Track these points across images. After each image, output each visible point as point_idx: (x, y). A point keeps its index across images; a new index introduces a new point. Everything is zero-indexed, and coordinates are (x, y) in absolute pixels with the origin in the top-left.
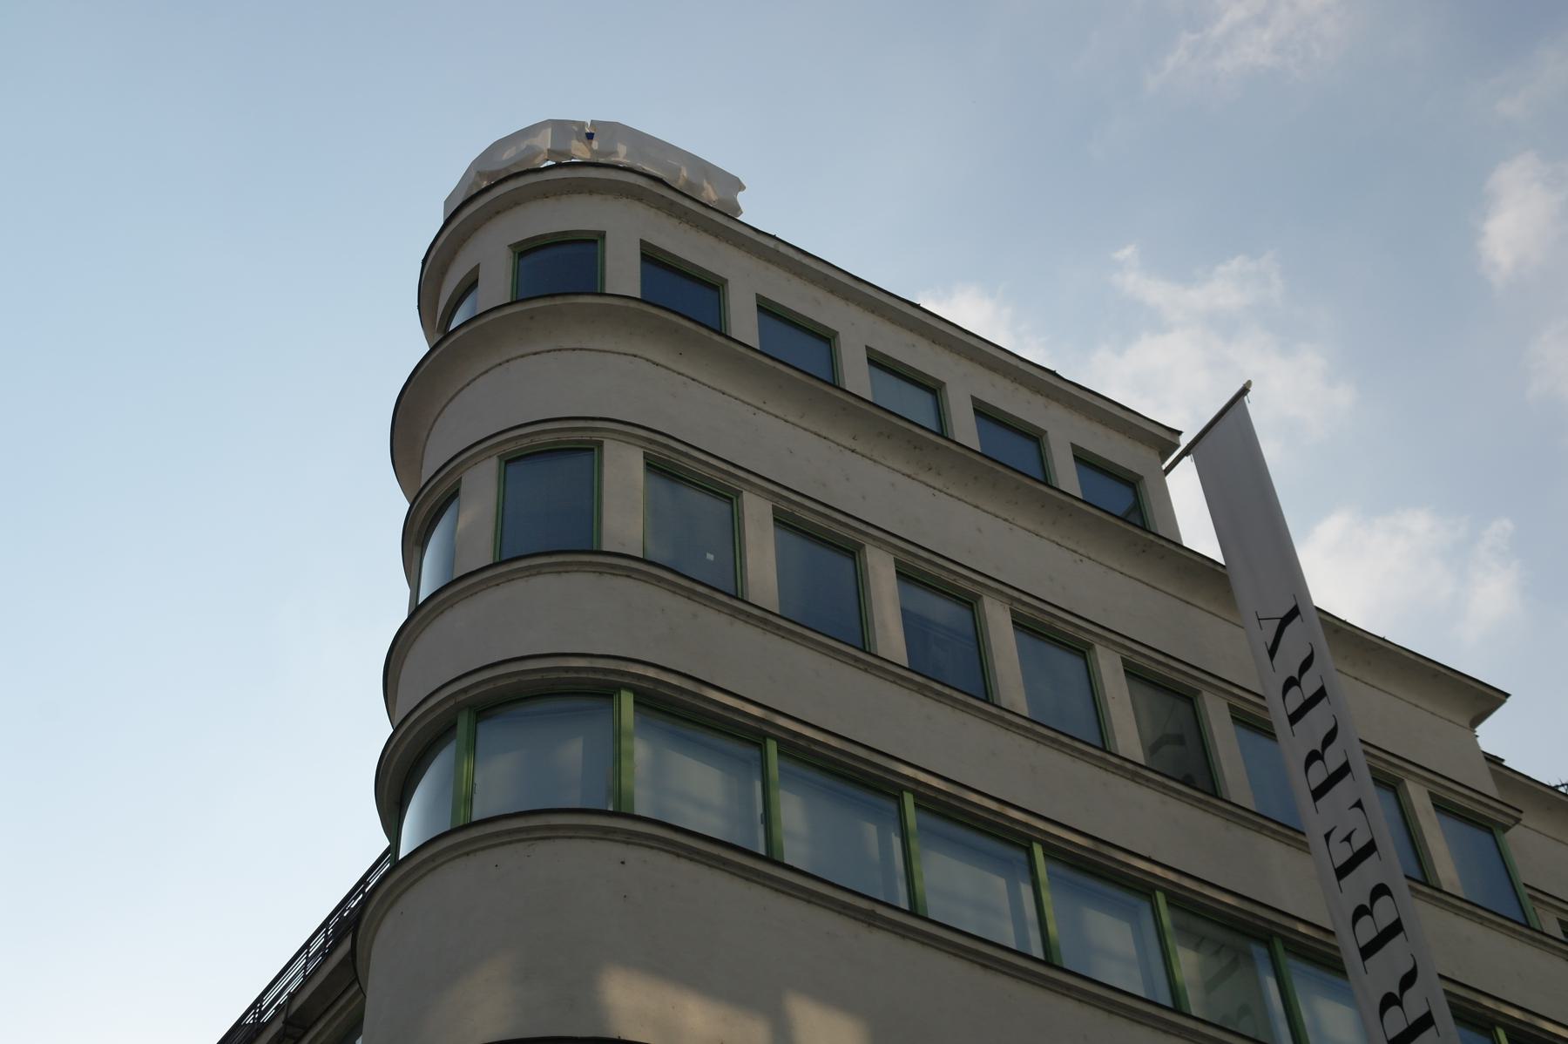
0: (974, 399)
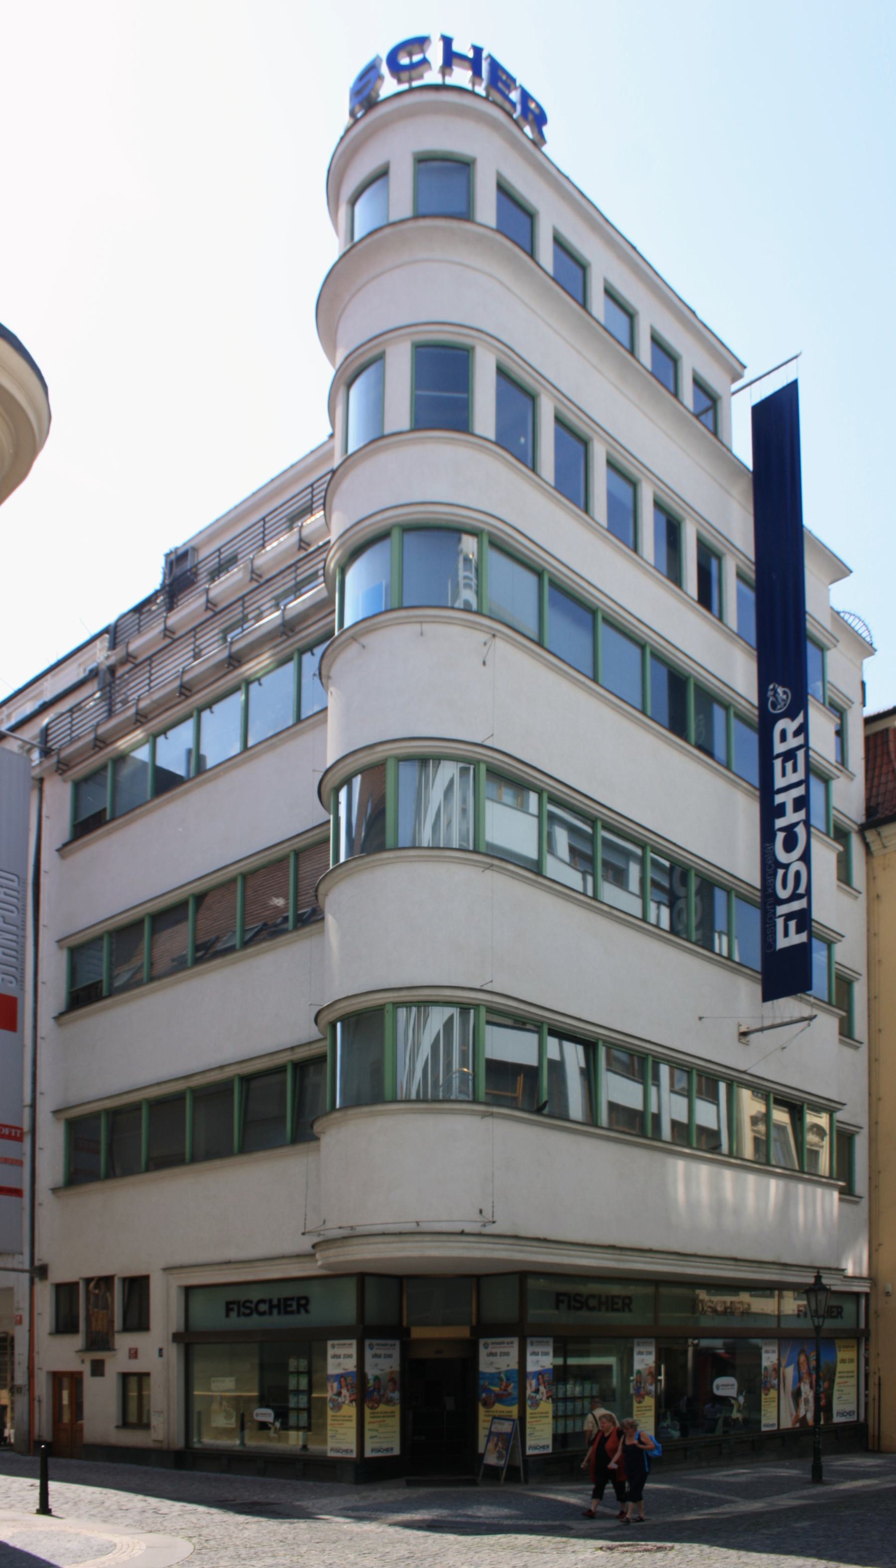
0: (606, 281)
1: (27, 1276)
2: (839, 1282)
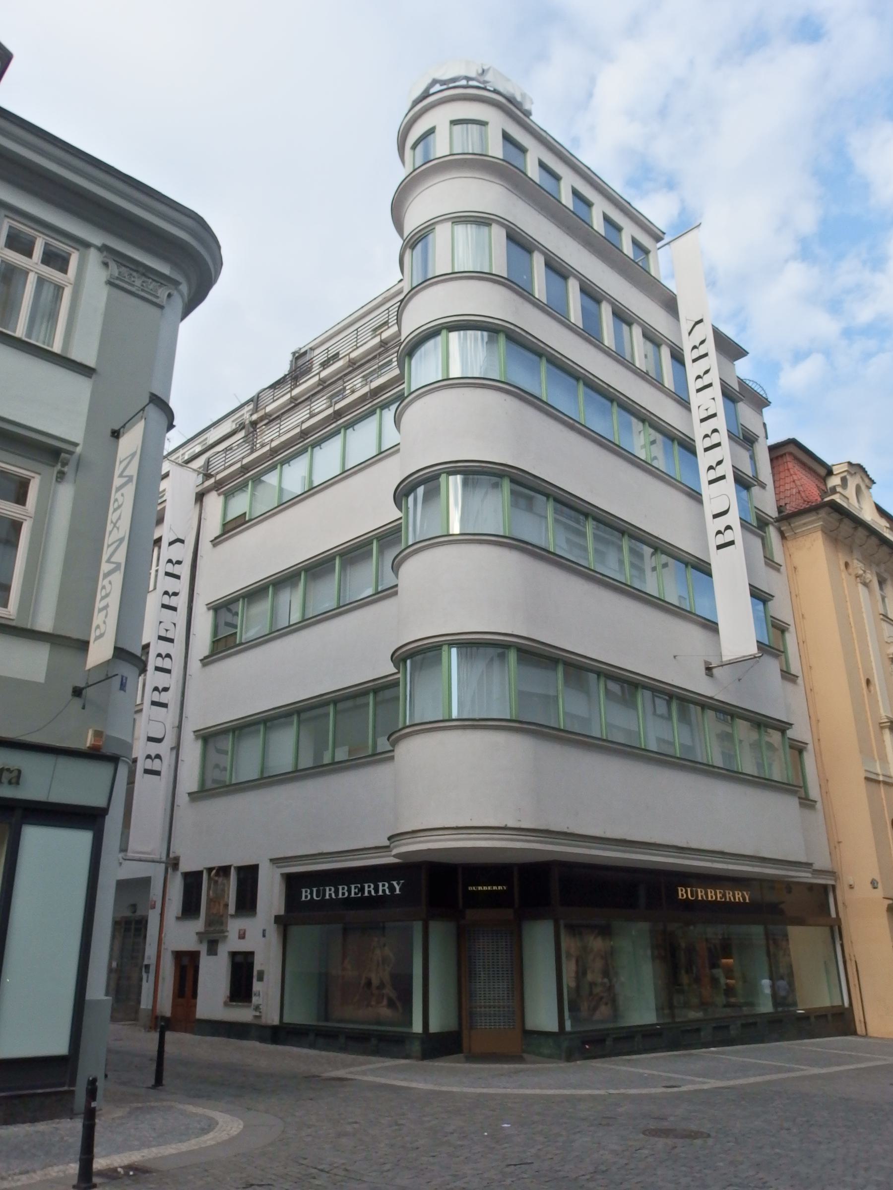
1: (163, 866)
2: (809, 875)
